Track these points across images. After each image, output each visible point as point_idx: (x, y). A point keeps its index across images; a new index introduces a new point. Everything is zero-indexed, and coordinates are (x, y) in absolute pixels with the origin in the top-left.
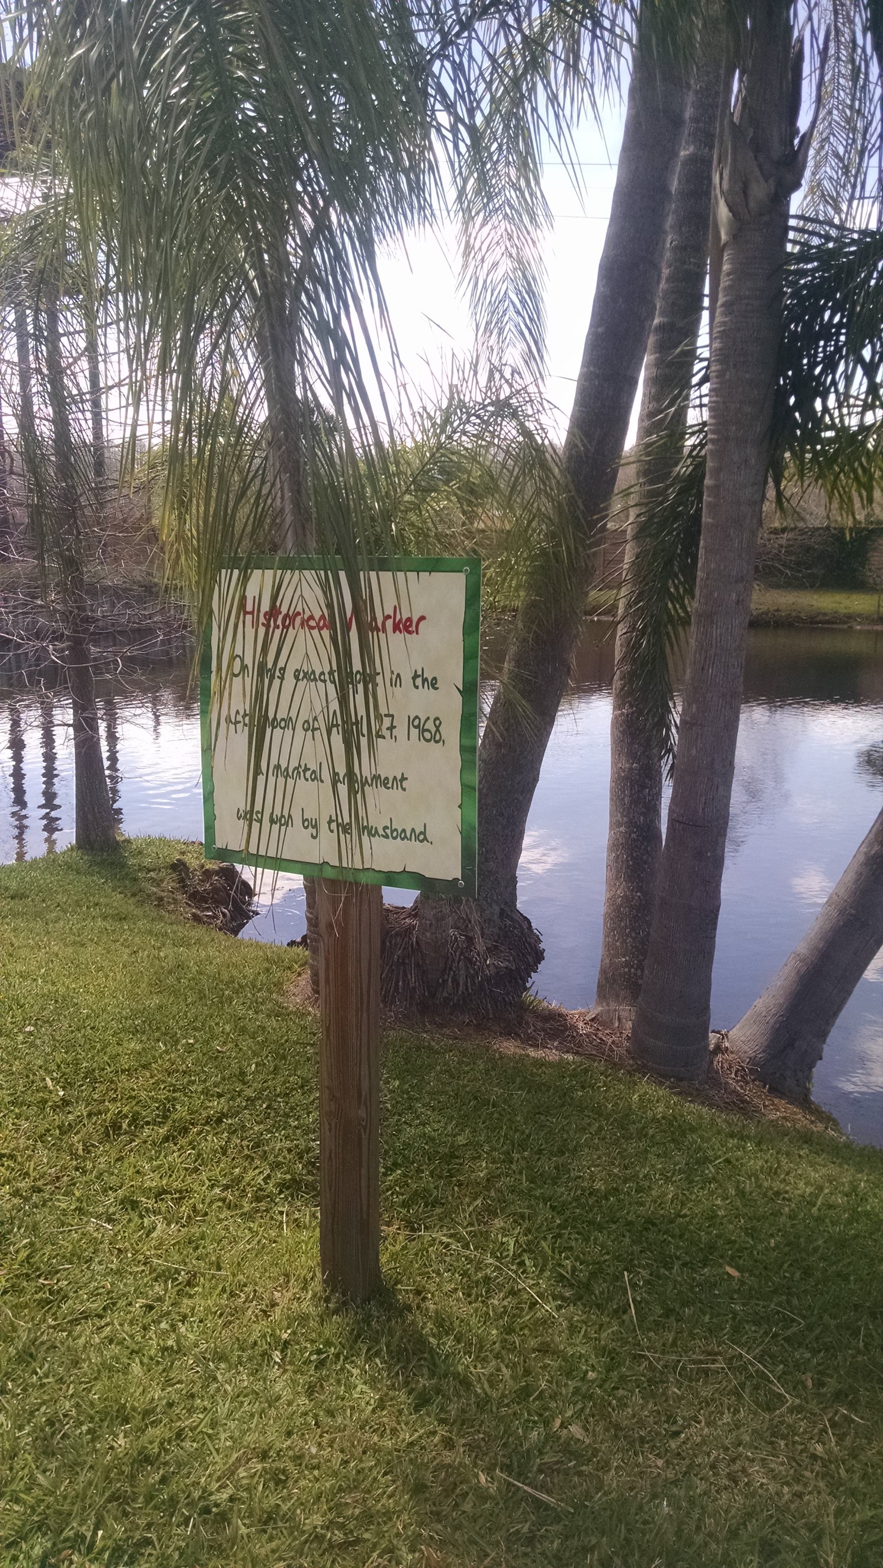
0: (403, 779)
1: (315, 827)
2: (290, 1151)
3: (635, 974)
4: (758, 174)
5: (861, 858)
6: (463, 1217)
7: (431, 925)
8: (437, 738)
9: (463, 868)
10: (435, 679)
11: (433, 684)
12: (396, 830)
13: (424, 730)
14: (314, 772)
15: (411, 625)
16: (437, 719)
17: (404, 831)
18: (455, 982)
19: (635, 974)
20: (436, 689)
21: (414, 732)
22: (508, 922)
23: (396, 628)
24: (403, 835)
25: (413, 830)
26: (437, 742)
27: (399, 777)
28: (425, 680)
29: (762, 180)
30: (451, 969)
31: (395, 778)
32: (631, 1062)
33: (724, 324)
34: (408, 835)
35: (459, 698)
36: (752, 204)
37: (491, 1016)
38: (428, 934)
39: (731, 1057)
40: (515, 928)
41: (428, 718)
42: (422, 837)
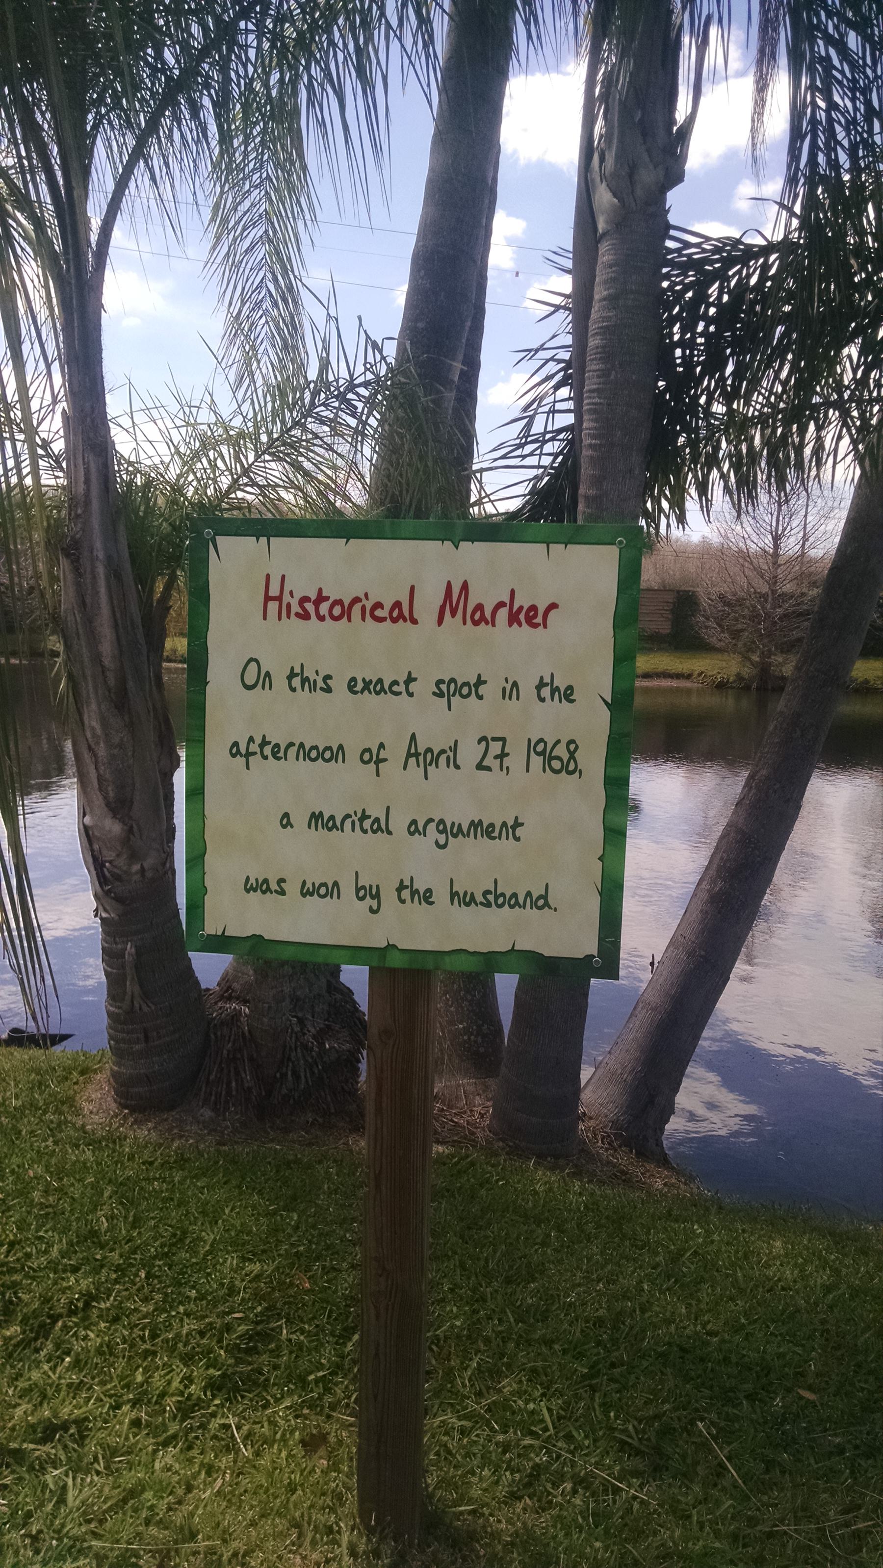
0: (517, 824)
1: (377, 896)
2: (202, 1334)
3: (476, 1042)
4: (647, 159)
5: (704, 896)
6: (463, 1381)
7: (270, 1007)
8: (572, 767)
9: (601, 940)
10: (570, 688)
11: (568, 695)
12: (503, 895)
13: (551, 758)
14: (377, 820)
15: (535, 616)
16: (572, 742)
17: (515, 895)
18: (296, 1076)
19: (476, 1042)
20: (572, 701)
21: (537, 761)
22: (338, 996)
23: (513, 619)
24: (513, 901)
25: (529, 894)
26: (570, 773)
27: (510, 823)
28: (554, 690)
29: (651, 167)
30: (289, 1059)
31: (504, 824)
32: (501, 1144)
33: (604, 319)
34: (521, 901)
35: (606, 714)
36: (639, 192)
37: (333, 1111)
38: (265, 1020)
39: (592, 1123)
40: (346, 1002)
41: (558, 742)
42: (541, 902)
